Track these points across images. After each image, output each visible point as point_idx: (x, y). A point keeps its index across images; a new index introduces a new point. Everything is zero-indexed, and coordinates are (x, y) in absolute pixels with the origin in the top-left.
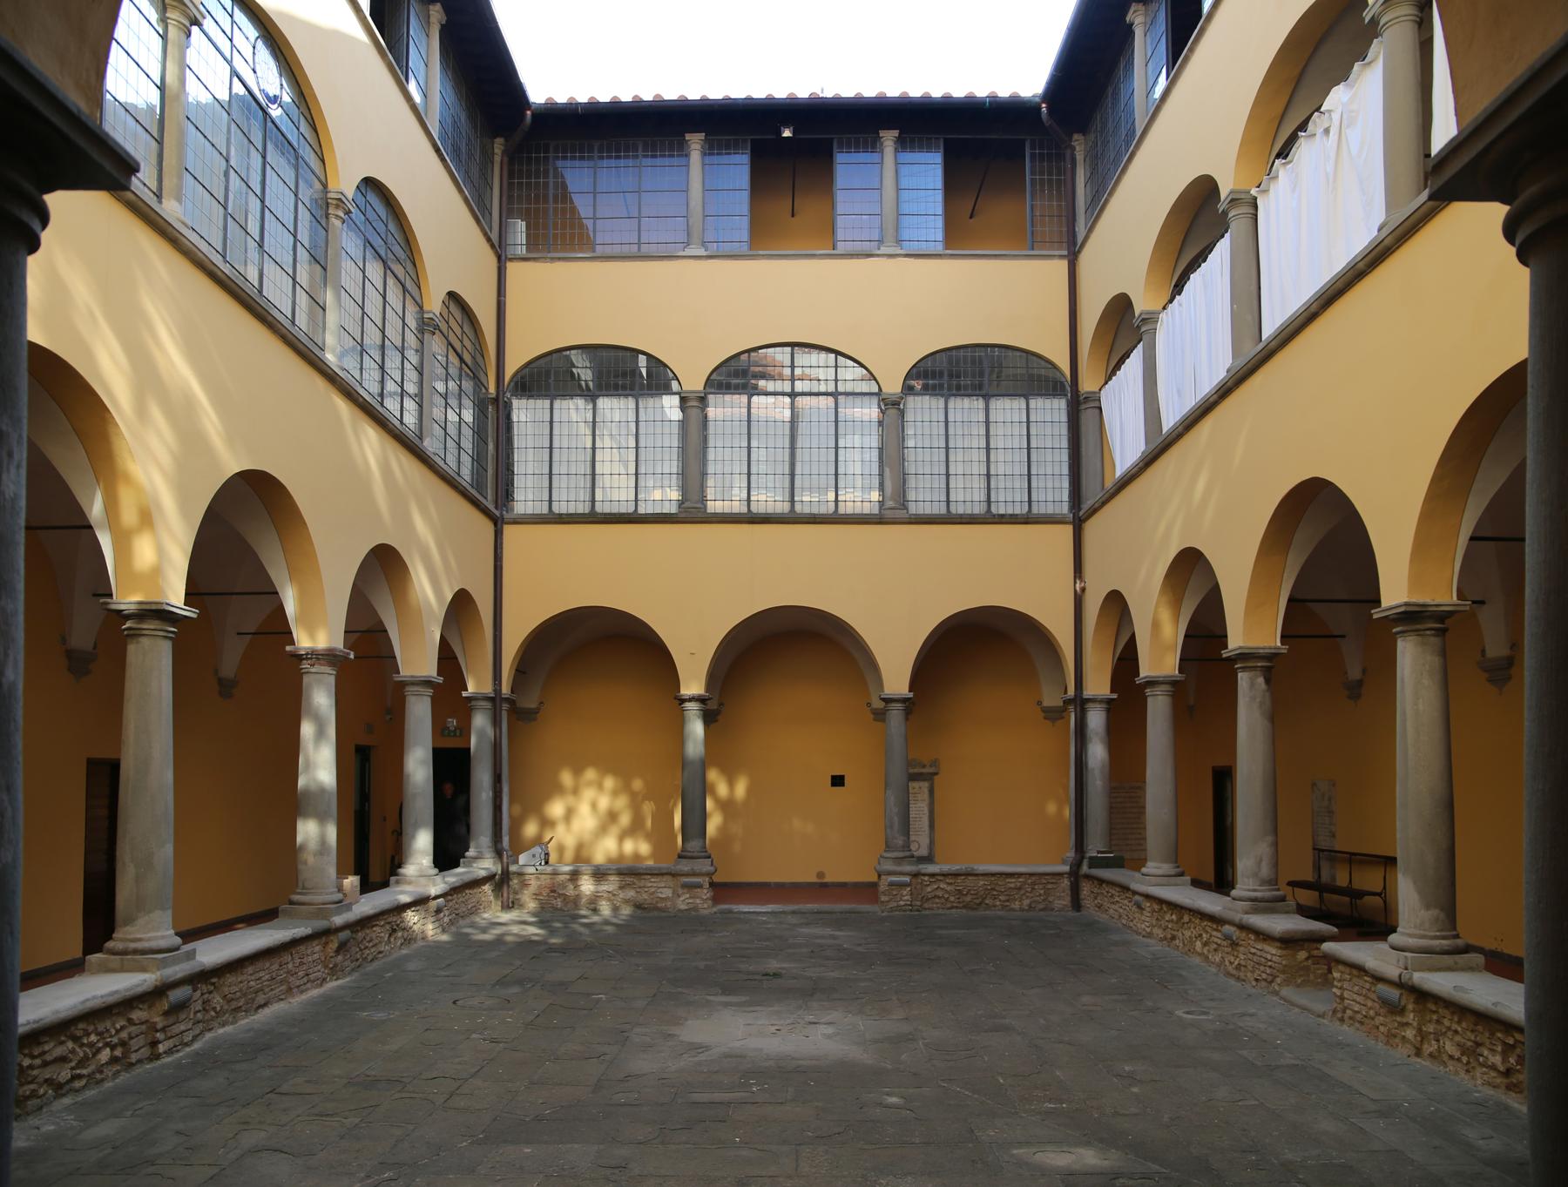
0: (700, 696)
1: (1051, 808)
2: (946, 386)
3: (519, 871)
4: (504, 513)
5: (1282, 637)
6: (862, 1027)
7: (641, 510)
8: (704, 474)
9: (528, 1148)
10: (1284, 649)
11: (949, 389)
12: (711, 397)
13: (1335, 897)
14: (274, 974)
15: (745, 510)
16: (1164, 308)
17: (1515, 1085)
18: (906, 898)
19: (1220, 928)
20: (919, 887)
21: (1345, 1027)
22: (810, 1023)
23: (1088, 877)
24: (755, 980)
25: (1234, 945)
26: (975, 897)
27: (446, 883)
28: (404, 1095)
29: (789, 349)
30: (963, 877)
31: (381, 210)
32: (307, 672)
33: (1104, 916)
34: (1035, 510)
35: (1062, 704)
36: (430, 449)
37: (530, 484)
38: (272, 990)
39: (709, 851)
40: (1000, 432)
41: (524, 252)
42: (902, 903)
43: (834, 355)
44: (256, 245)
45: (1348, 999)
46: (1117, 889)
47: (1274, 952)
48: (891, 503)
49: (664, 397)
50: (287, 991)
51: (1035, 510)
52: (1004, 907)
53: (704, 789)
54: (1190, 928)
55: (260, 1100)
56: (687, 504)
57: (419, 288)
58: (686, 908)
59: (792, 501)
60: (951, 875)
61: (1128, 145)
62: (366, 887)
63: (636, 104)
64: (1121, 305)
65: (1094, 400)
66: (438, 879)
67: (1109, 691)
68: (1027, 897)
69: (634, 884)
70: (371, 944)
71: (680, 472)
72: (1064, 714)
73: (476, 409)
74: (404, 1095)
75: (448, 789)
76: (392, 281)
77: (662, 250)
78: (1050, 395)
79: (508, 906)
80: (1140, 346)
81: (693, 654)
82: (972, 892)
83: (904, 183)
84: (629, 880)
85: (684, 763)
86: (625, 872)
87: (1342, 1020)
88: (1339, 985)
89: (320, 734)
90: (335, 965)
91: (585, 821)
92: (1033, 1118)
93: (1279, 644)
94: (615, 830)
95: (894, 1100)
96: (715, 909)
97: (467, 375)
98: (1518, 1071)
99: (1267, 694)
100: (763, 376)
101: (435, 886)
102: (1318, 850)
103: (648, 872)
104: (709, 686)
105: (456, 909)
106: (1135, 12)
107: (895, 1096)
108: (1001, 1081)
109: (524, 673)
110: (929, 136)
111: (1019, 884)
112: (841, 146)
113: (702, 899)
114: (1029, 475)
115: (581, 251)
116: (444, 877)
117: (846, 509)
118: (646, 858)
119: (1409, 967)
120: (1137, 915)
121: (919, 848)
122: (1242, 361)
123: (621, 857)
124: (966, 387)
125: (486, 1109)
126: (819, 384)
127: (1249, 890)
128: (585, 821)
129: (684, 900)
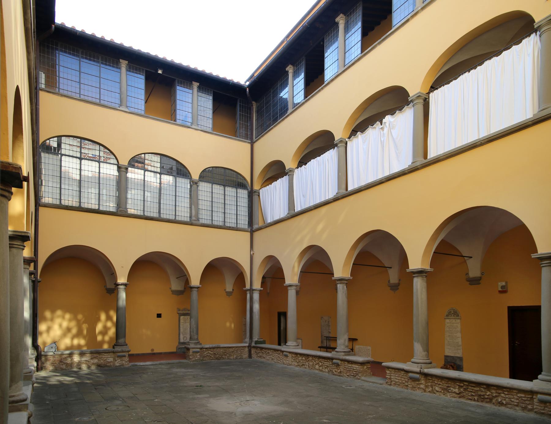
0: (126, 283)
1: (228, 324)
10: (351, 278)
17: (463, 396)
18: (198, 357)
39: (127, 343)
42: (197, 358)
47: (357, 367)
58: (119, 365)
60: (212, 348)
63: (111, 42)
67: (199, 284)
69: (97, 357)
78: (234, 187)
82: (219, 354)
84: (95, 355)
91: (56, 332)
94: (70, 335)
98: (463, 393)
99: (347, 291)
103: (104, 352)
106: (290, 68)
111: (233, 350)
113: (126, 361)
119: (423, 368)
127: (342, 349)
128: (56, 332)
129: (118, 362)
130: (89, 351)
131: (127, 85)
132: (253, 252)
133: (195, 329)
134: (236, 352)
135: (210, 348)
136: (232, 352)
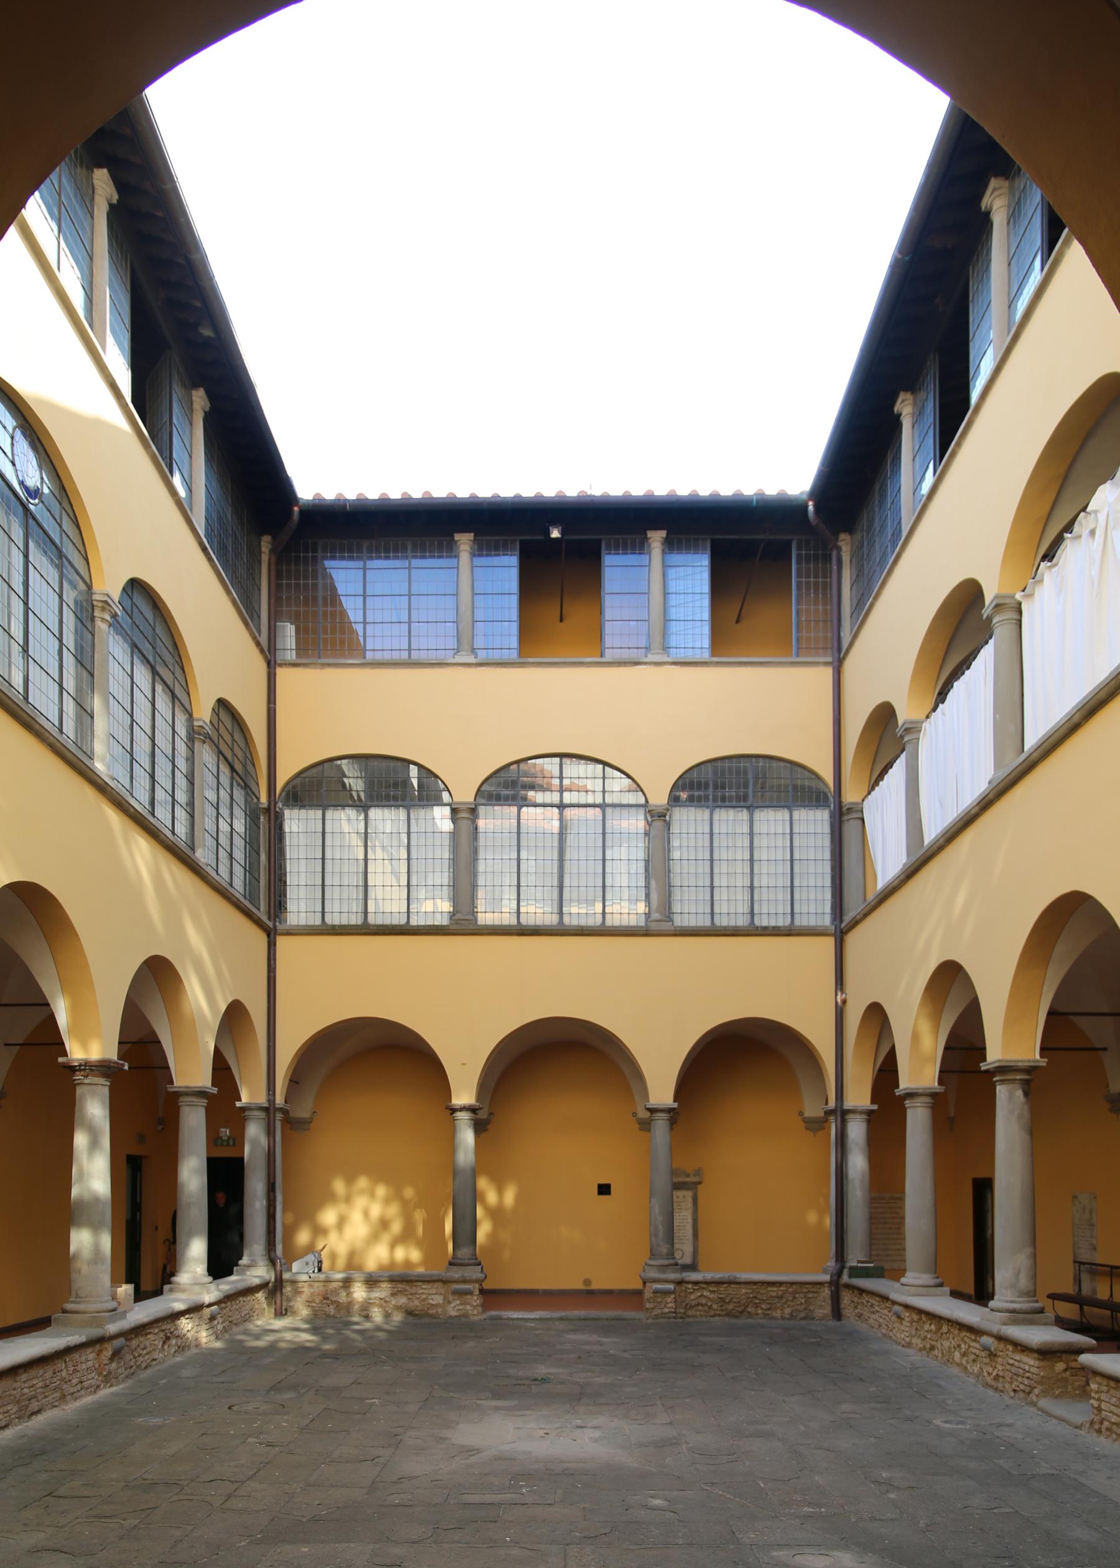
0: (470, 1106)
2: (711, 797)
3: (292, 1278)
4: (277, 924)
5: (1042, 1049)
6: (627, 1431)
7: (414, 922)
8: (474, 886)
9: (305, 1548)
10: (1043, 1062)
11: (715, 800)
12: (482, 810)
13: (1096, 1310)
14: (48, 1382)
15: (514, 922)
16: (928, 717)
18: (670, 1305)
19: (978, 1338)
20: (683, 1294)
21: (1102, 1438)
22: (578, 1427)
23: (848, 1286)
24: (524, 1385)
25: (992, 1355)
26: (737, 1305)
27: (220, 1291)
28: (182, 1497)
29: (558, 759)
30: (725, 1285)
31: (148, 613)
32: (81, 1084)
33: (864, 1325)
34: (797, 922)
35: (823, 1115)
36: (203, 860)
37: (302, 895)
38: (45, 1397)
39: (480, 1258)
40: (764, 843)
41: (294, 657)
42: (666, 1310)
43: (601, 766)
44: (21, 649)
45: (1105, 1411)
46: (877, 1299)
47: (1032, 1362)
48: (657, 915)
49: (435, 808)
50: (60, 1398)
51: (797, 922)
52: (765, 1315)
53: (475, 1196)
54: (949, 1338)
55: (37, 1503)
56: (458, 916)
57: (188, 694)
59: (561, 913)
61: (894, 546)
62: (140, 1296)
64: (884, 715)
65: (856, 812)
66: (213, 1287)
68: (789, 1306)
70: (145, 1352)
71: (451, 884)
72: (825, 1125)
73: (248, 818)
74: (182, 1497)
75: (221, 1198)
76: (161, 687)
77: (432, 656)
79: (280, 1313)
80: (903, 756)
81: (463, 1064)
82: (735, 1300)
83: (673, 586)
84: (401, 1286)
85: (455, 1172)
86: (396, 1279)
87: (1099, 1431)
88: (1097, 1396)
89: (94, 1144)
90: (110, 1373)
91: (358, 1229)
92: (793, 1522)
93: (1038, 1057)
94: (386, 1238)
95: (657, 1502)
96: (484, 1316)
97: (238, 784)
99: (1026, 1107)
100: (532, 787)
101: (208, 1293)
102: (1079, 1263)
103: (420, 1279)
104: (480, 1096)
105: (229, 1317)
107: (660, 1499)
108: (762, 1485)
109: (298, 1083)
110: (696, 536)
111: (780, 1293)
112: (609, 548)
113: (472, 1305)
114: (792, 887)
115: (351, 657)
116: (218, 1285)
117: (613, 921)
118: (417, 1265)
120: (896, 1325)
121: (683, 1253)
122: (1003, 773)
123: (393, 1264)
124: (731, 799)
125: (263, 1510)
126: (587, 795)
127: (1007, 1302)
130: (387, 1275)
131: (474, 594)
132: (844, 996)
133: (661, 1227)
134: (790, 1299)
135: (708, 1283)
136: (778, 1297)
